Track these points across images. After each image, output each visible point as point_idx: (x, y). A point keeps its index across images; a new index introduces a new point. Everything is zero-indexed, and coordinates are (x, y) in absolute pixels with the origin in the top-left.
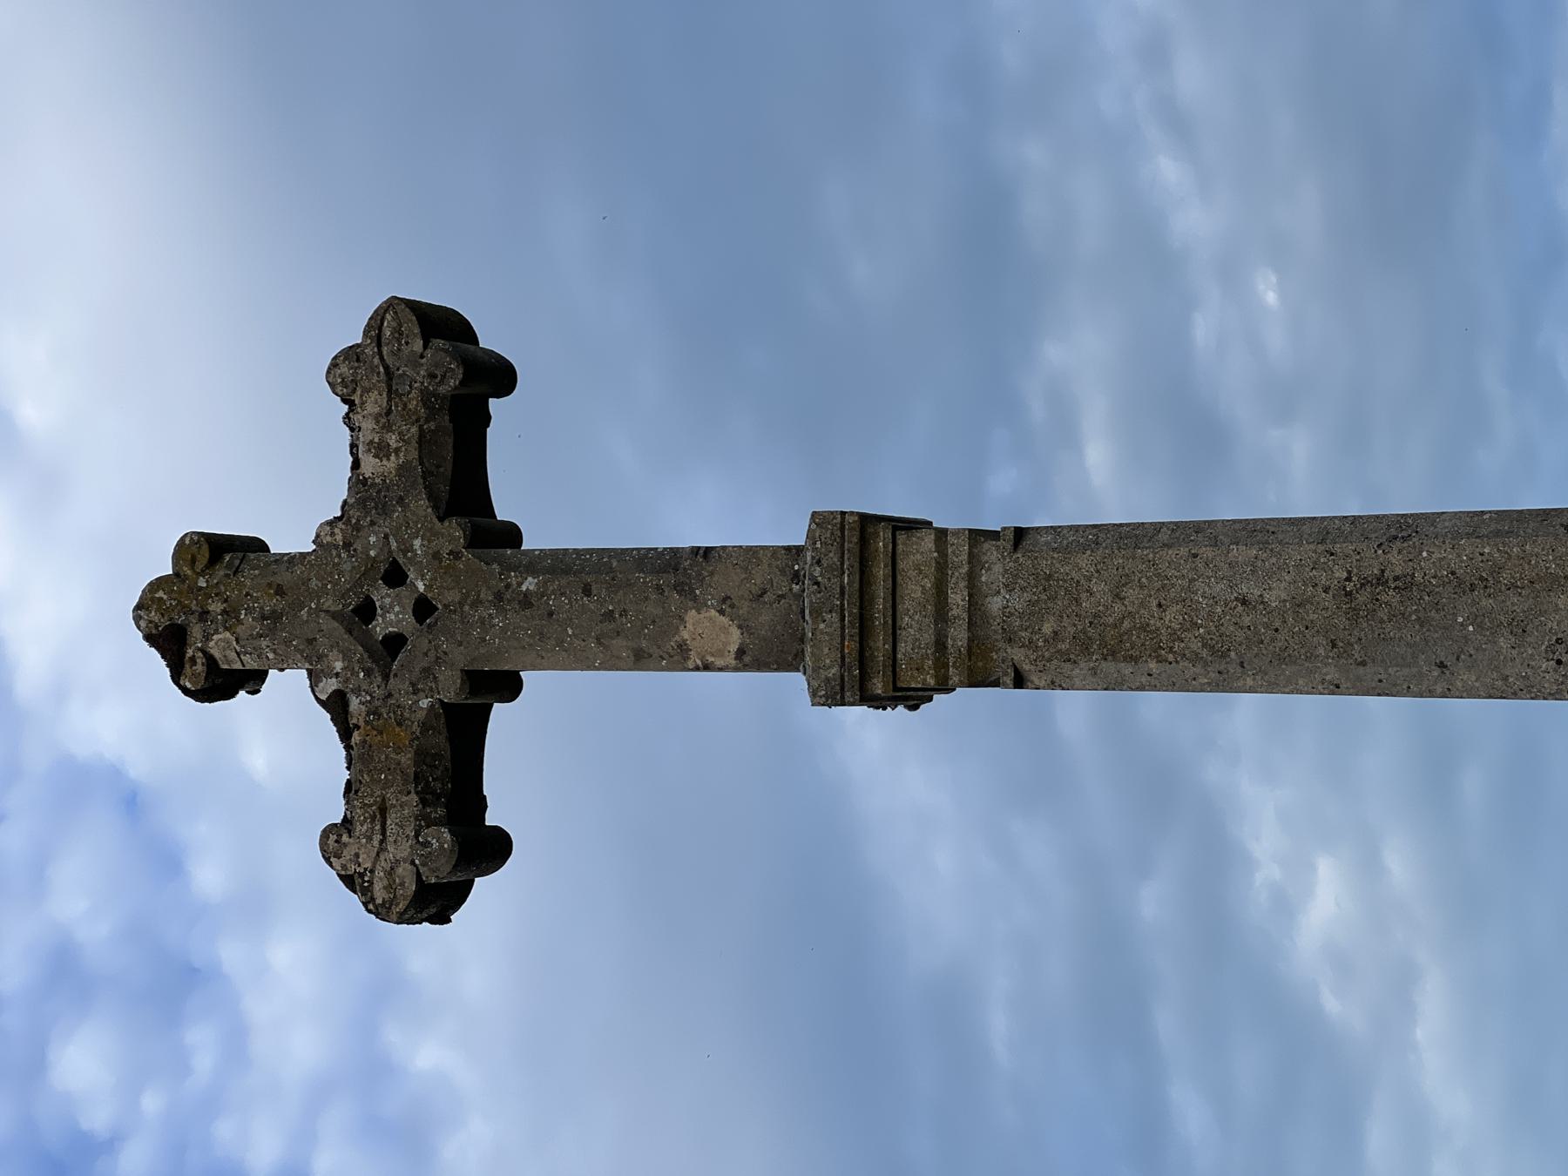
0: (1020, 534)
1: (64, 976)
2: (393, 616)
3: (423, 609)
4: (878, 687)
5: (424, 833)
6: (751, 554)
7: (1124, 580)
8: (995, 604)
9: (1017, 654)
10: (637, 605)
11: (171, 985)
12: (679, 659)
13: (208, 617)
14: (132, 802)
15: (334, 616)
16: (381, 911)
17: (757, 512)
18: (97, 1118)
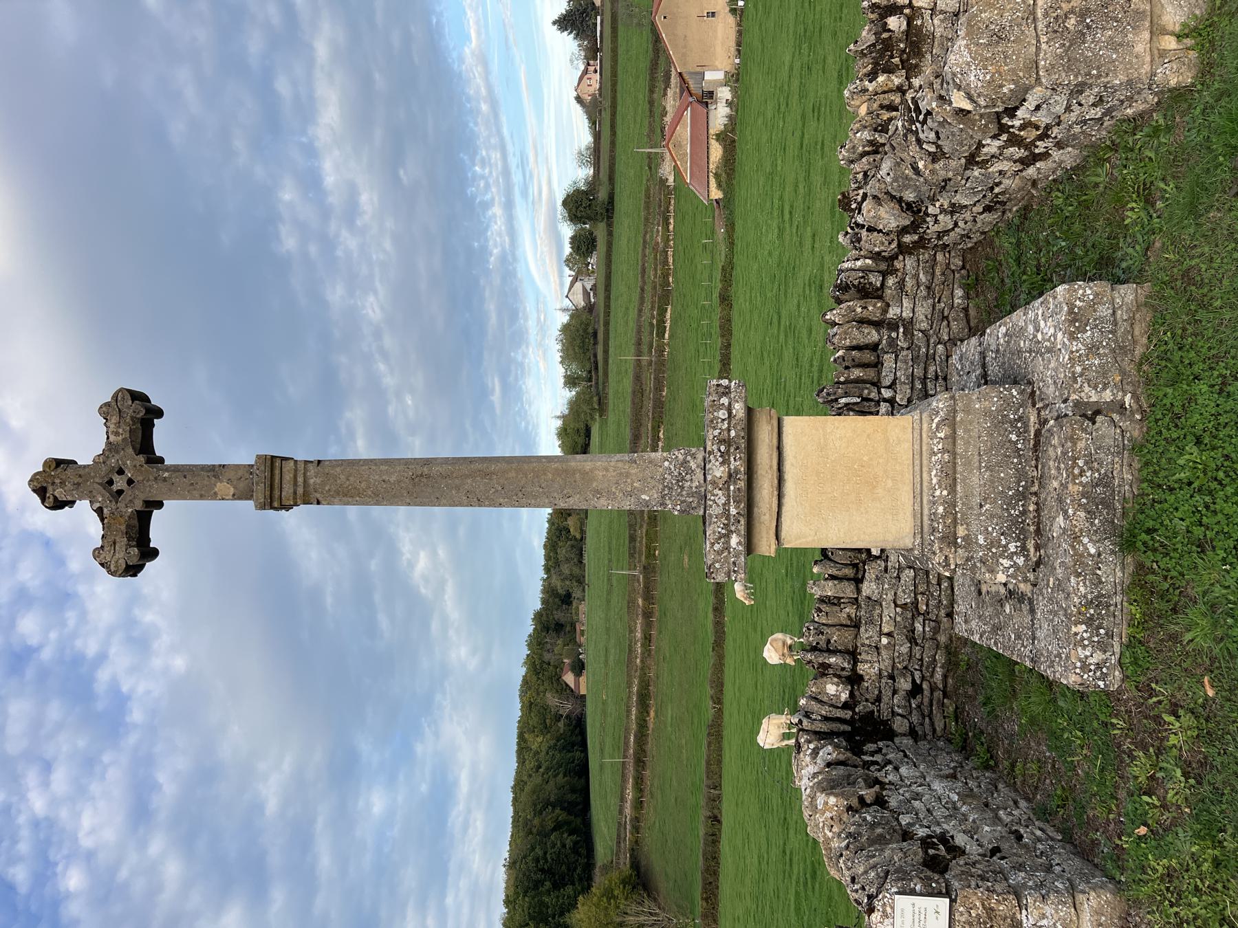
0: (319, 462)
1: (23, 599)
2: (120, 483)
3: (130, 482)
4: (276, 504)
5: (132, 548)
6: (238, 466)
7: (350, 475)
8: (312, 481)
9: (318, 495)
10: (201, 481)
11: (60, 599)
12: (214, 496)
13: (55, 484)
14: (47, 543)
15: (100, 484)
16: (113, 574)
17: (244, 456)
18: (34, 641)
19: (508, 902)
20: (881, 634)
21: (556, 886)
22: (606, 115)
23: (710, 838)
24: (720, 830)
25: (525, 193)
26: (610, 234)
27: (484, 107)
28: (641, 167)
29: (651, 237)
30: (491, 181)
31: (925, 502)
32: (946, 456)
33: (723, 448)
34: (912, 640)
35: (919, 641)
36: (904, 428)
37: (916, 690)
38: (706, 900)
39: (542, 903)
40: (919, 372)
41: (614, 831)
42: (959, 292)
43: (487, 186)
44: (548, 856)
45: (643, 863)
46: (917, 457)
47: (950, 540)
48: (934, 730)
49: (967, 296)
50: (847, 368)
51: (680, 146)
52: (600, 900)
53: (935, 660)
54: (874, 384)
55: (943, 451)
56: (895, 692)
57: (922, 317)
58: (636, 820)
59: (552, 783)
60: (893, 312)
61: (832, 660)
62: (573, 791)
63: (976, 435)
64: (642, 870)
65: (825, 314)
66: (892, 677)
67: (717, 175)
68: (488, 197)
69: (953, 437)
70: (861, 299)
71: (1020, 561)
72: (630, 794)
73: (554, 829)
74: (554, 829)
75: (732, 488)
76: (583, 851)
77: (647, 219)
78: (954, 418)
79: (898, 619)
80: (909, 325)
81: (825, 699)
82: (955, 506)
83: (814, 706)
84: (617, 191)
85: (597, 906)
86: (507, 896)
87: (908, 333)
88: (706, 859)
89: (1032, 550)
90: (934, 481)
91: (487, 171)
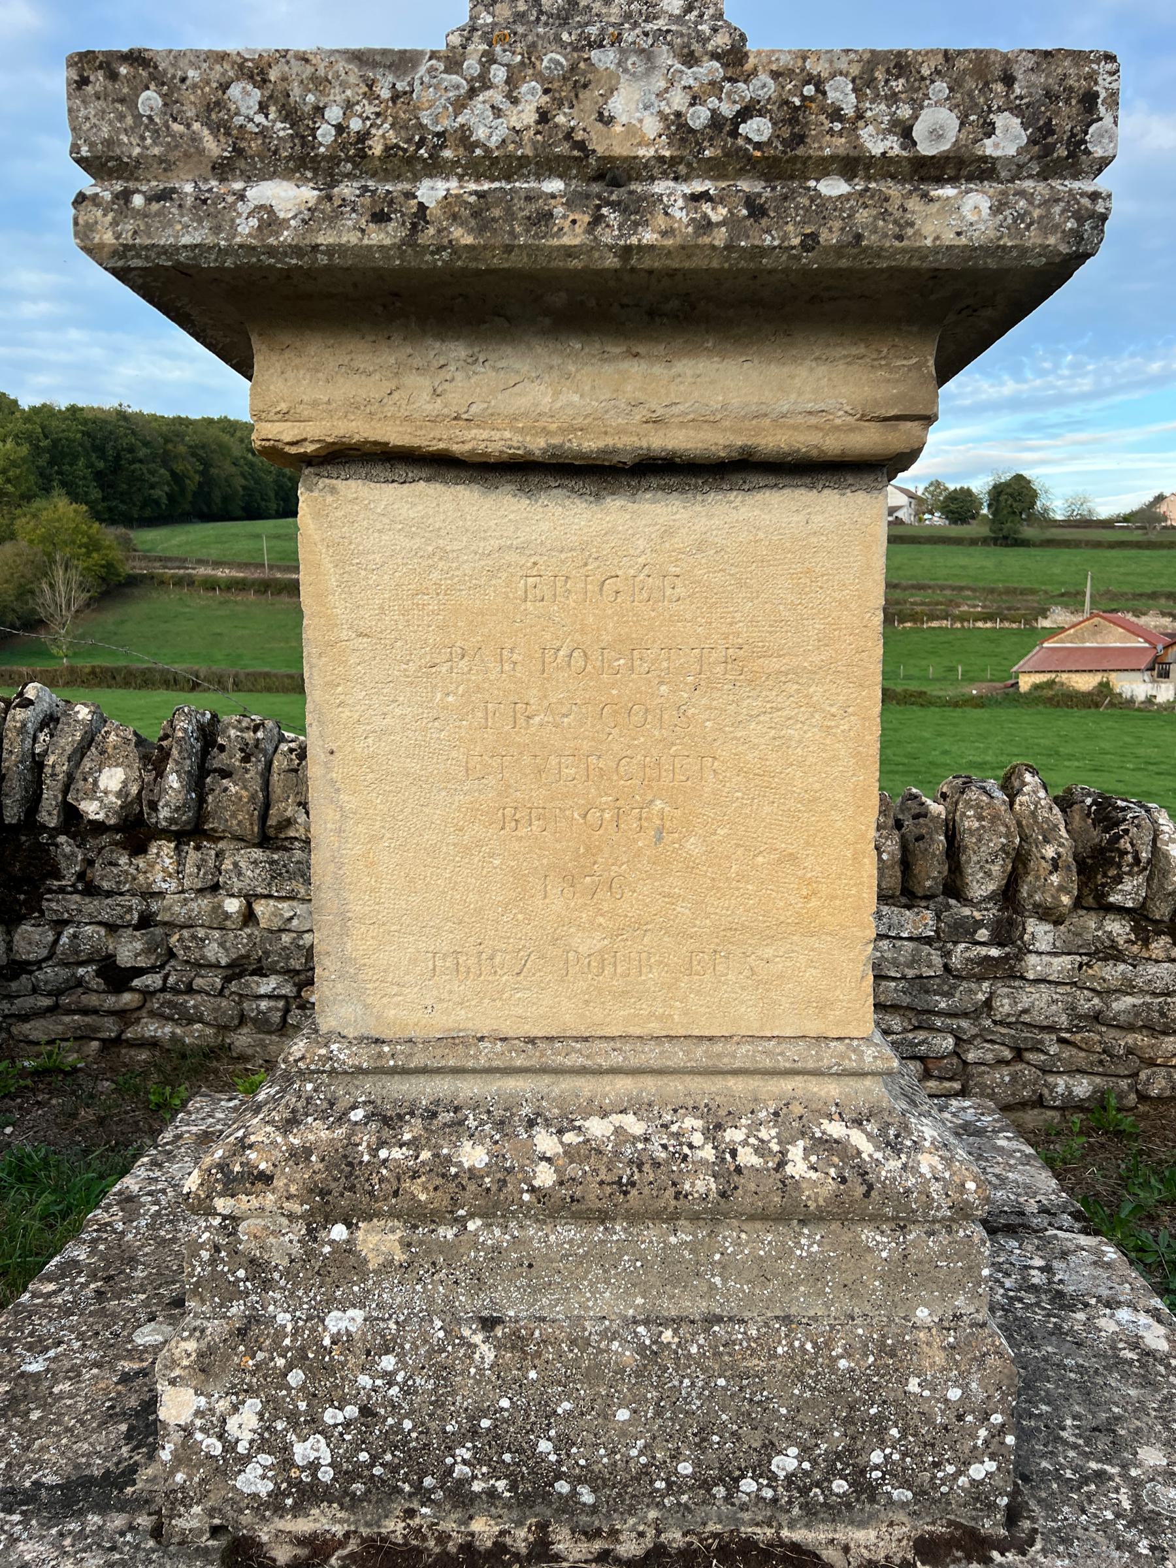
19: (73, 410)
20: (250, 898)
21: (99, 475)
22: (1137, 536)
23: (171, 677)
24: (182, 689)
25: (1031, 427)
26: (973, 542)
27: (1155, 367)
28: (1063, 583)
29: (968, 598)
30: (1051, 378)
31: (511, 1084)
32: (703, 1185)
33: (758, 129)
34: (237, 969)
35: (233, 986)
36: (824, 1006)
37: (117, 977)
38: (93, 672)
39: (75, 457)
41: (175, 553)
42: (1082, 1088)
43: (1042, 373)
44: (137, 466)
45: (136, 592)
46: (700, 1055)
47: (341, 1191)
48: (25, 1018)
49: (1070, 1105)
51: (1095, 634)
52: (84, 534)
53: (191, 1021)
55: (728, 1172)
56: (112, 928)
57: (1025, 1001)
58: (190, 582)
59: (234, 469)
60: (1040, 933)
61: (173, 780)
62: (226, 499)
63: (806, 1303)
64: (127, 590)
65: (1034, 772)
66: (146, 921)
67: (1052, 683)
68: (1029, 374)
69: (789, 1211)
70: (1075, 856)
71: (254, 1480)
72: (223, 573)
73: (173, 473)
74: (173, 473)
75: (554, 185)
76: (148, 512)
77: (992, 591)
78: (875, 1220)
79: (286, 938)
80: (1007, 970)
81: (87, 764)
82: (485, 1214)
83: (69, 739)
84: (1033, 551)
85: (76, 530)
86: (82, 409)
87: (987, 969)
88: (143, 672)
89: (303, 1526)
90: (598, 1128)
91: (1066, 372)
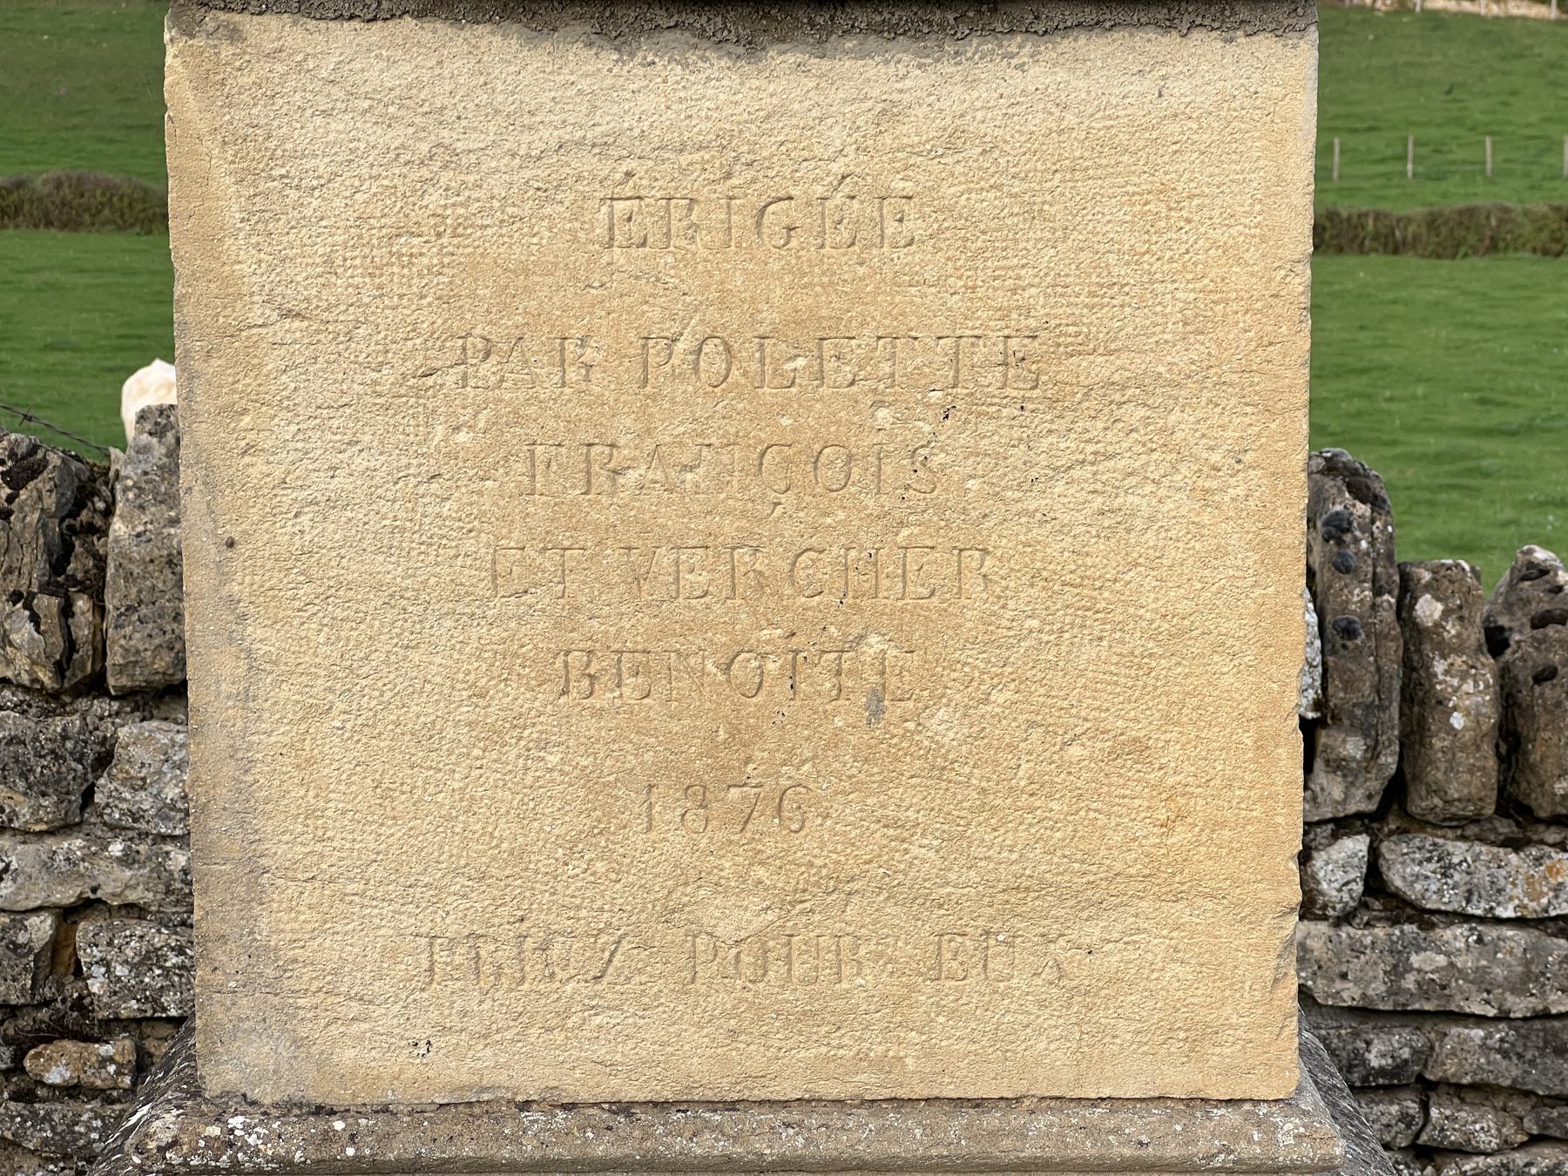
36: (1200, 1037)
40: (1465, 1051)
50: (1496, 641)
54: (1396, 793)
